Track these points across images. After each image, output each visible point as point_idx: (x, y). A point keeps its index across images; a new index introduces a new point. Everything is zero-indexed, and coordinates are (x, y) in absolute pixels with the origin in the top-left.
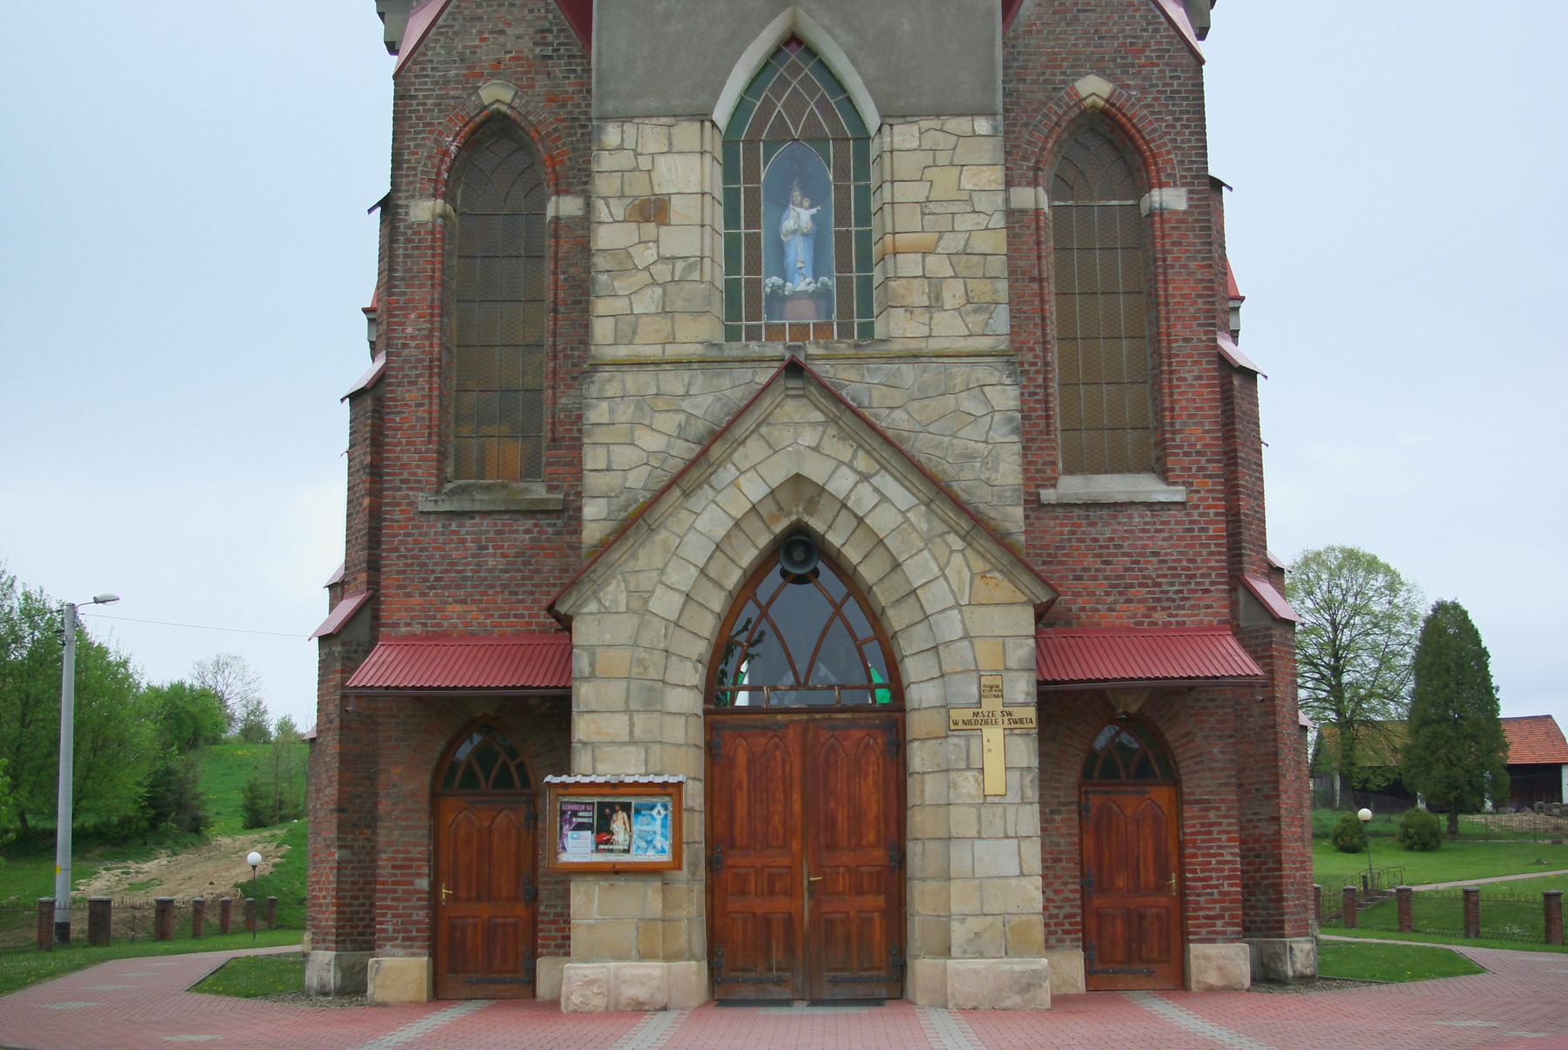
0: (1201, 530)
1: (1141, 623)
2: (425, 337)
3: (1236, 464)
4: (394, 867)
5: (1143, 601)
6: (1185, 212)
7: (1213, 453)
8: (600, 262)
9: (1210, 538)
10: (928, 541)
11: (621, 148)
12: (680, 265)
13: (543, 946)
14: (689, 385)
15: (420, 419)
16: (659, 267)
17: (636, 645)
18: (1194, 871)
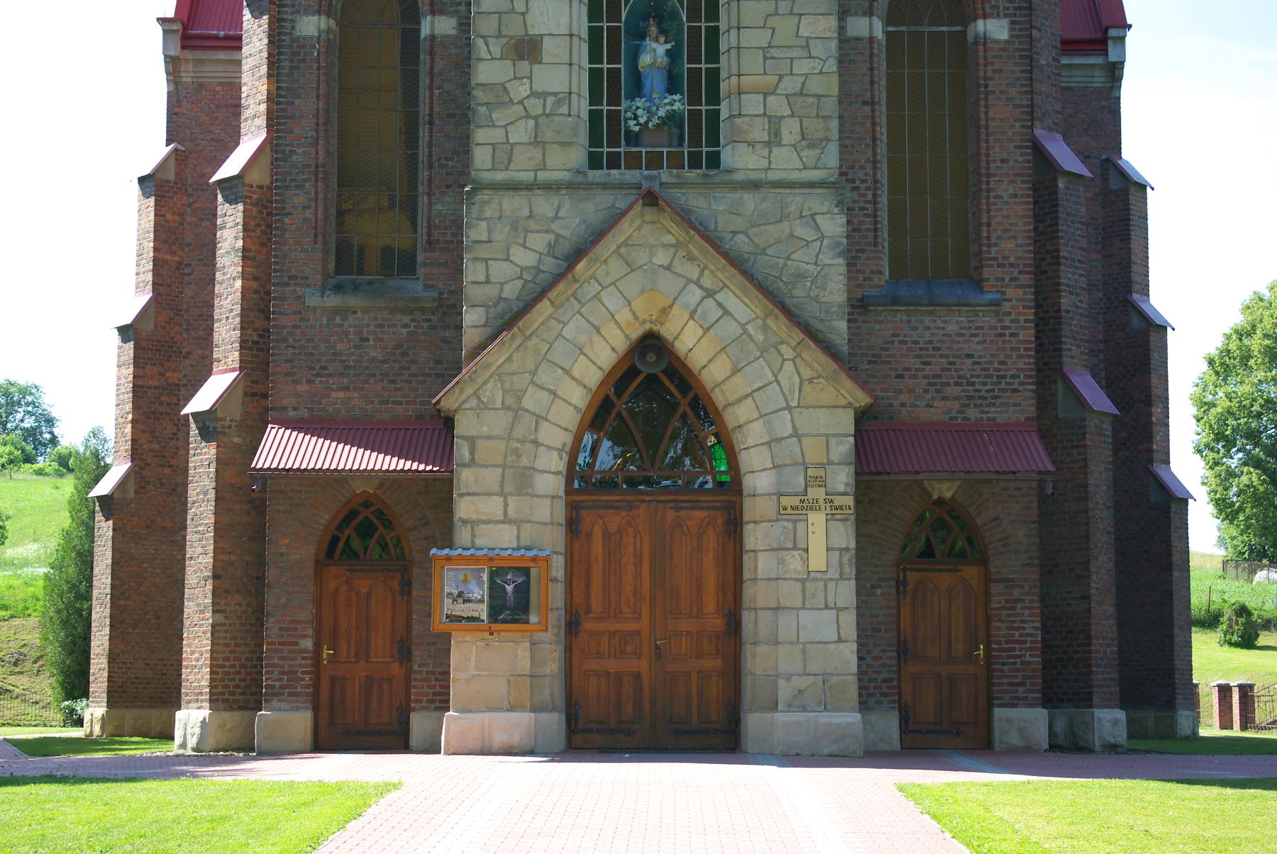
0: (1012, 335)
1: (956, 418)
2: (312, 144)
3: (1058, 264)
4: (281, 629)
5: (957, 398)
6: (1007, 42)
8: (479, 94)
10: (763, 351)
12: (550, 100)
13: (415, 701)
14: (559, 208)
15: (305, 220)
16: (532, 100)
17: (509, 438)
18: (999, 643)
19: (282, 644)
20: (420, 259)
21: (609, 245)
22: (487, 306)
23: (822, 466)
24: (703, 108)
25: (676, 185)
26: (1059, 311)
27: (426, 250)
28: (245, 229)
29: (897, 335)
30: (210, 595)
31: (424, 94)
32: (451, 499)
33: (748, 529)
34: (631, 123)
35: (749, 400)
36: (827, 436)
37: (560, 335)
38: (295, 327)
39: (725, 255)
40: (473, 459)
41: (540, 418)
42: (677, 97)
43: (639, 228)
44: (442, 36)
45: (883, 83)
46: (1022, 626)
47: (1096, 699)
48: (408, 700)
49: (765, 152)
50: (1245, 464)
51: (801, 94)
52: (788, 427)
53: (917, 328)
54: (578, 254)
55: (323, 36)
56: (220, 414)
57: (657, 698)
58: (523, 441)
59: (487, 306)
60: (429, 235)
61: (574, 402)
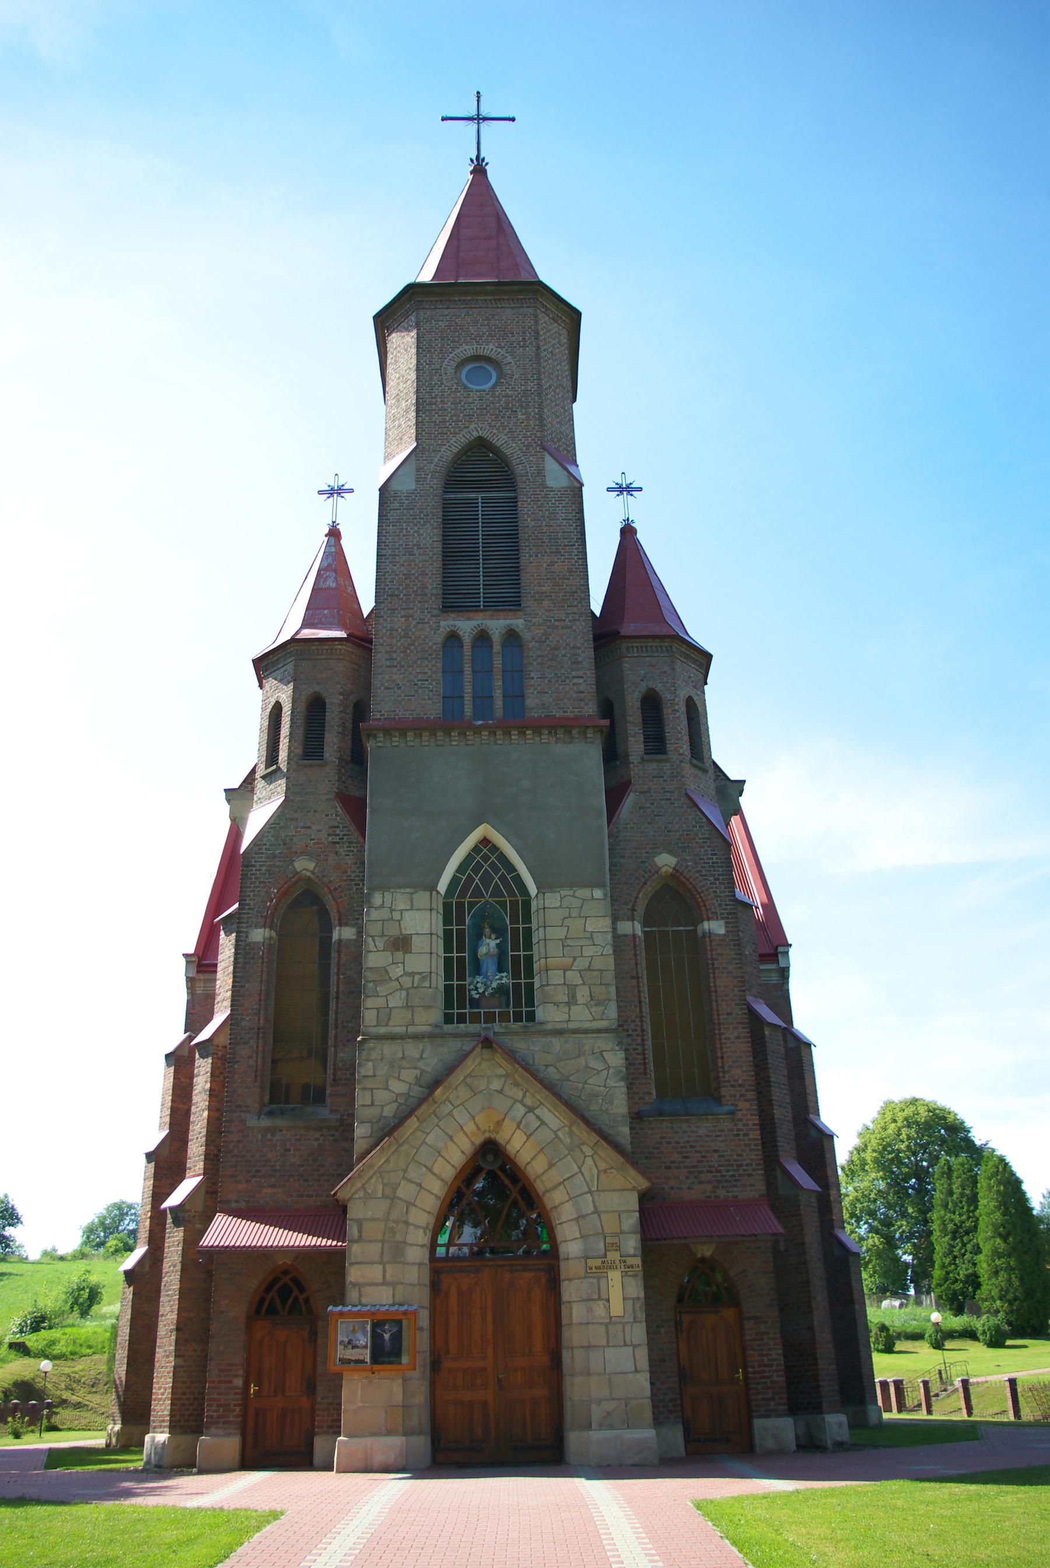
0: (745, 1135)
1: (709, 1197)
3: (770, 1086)
5: (710, 1182)
7: (750, 1085)
8: (369, 975)
9: (751, 1140)
10: (571, 1150)
11: (382, 906)
12: (417, 977)
16: (405, 978)
18: (753, 1367)
19: (219, 1382)
20: (328, 1092)
21: (459, 1076)
22: (372, 1123)
23: (616, 1235)
24: (523, 981)
25: (504, 1034)
26: (773, 1119)
27: (332, 1085)
28: (212, 1075)
29: (664, 1138)
30: (173, 1343)
31: (333, 978)
32: (344, 1267)
33: (564, 1285)
34: (473, 993)
35: (561, 1187)
36: (619, 1213)
37: (424, 1142)
38: (239, 1142)
39: (541, 1082)
40: (360, 1237)
41: (410, 1204)
42: (505, 974)
43: (479, 1064)
44: (347, 940)
45: (644, 964)
46: (769, 1354)
47: (825, 1406)
48: (313, 1426)
49: (566, 1010)
50: (869, 1232)
51: (589, 969)
52: (591, 1205)
53: (677, 1132)
54: (436, 1083)
55: (267, 941)
56: (187, 1207)
57: (497, 1422)
58: (397, 1222)
59: (372, 1123)
60: (334, 1074)
61: (434, 1192)
